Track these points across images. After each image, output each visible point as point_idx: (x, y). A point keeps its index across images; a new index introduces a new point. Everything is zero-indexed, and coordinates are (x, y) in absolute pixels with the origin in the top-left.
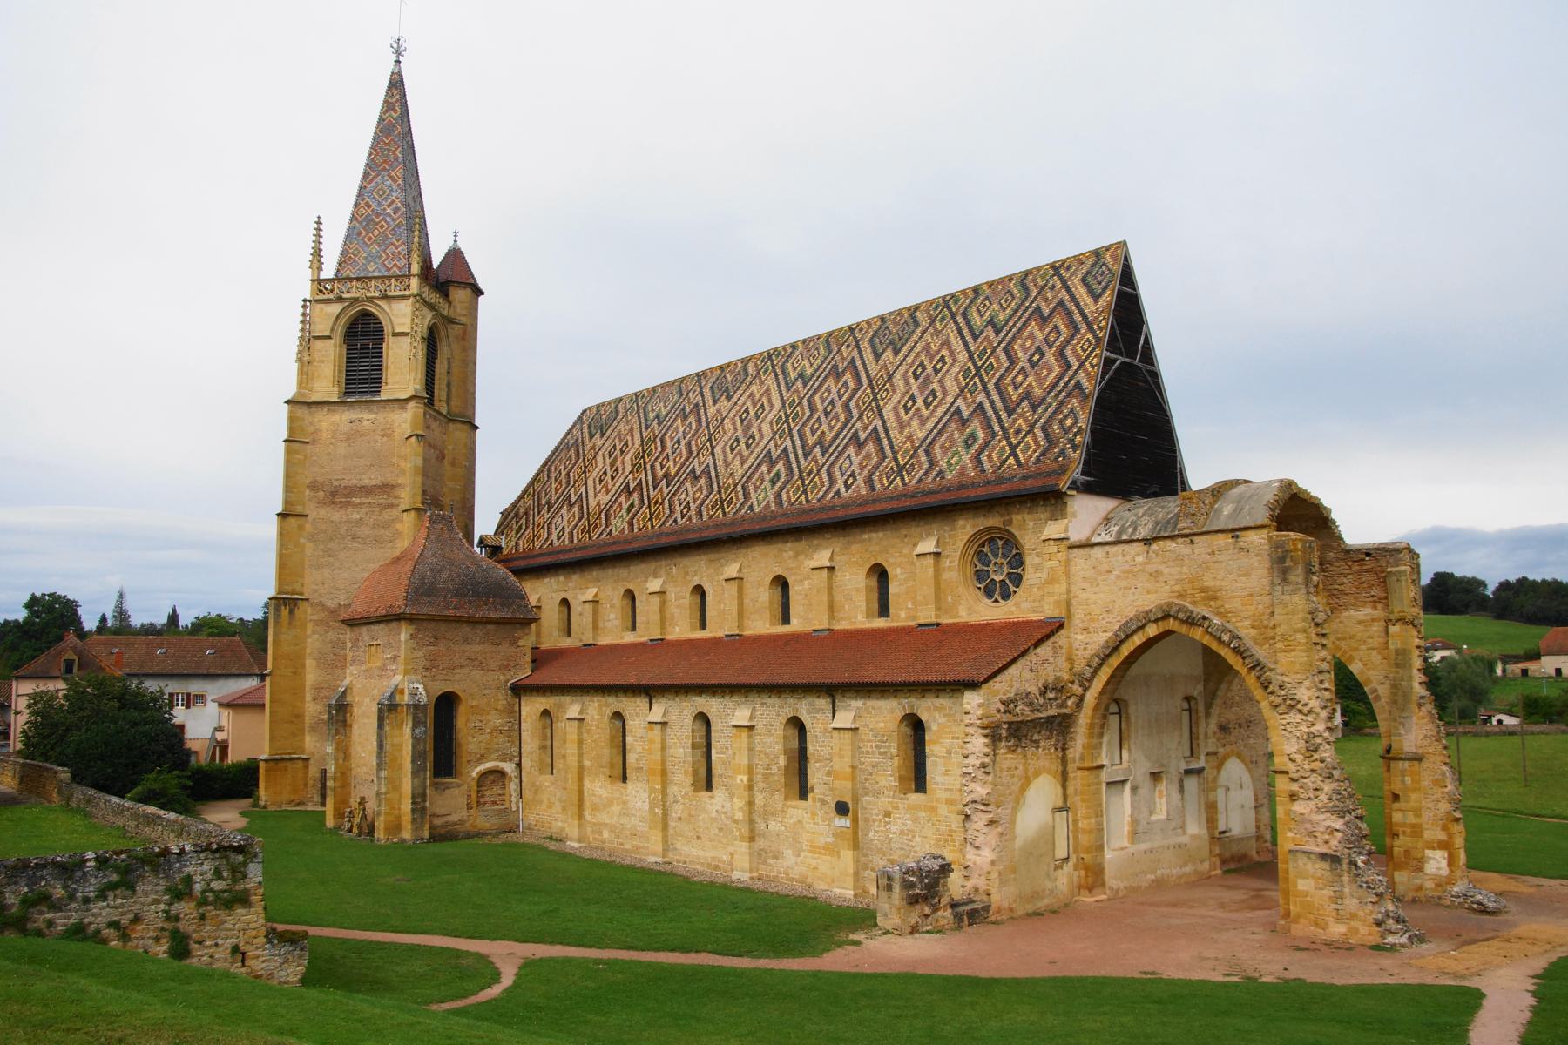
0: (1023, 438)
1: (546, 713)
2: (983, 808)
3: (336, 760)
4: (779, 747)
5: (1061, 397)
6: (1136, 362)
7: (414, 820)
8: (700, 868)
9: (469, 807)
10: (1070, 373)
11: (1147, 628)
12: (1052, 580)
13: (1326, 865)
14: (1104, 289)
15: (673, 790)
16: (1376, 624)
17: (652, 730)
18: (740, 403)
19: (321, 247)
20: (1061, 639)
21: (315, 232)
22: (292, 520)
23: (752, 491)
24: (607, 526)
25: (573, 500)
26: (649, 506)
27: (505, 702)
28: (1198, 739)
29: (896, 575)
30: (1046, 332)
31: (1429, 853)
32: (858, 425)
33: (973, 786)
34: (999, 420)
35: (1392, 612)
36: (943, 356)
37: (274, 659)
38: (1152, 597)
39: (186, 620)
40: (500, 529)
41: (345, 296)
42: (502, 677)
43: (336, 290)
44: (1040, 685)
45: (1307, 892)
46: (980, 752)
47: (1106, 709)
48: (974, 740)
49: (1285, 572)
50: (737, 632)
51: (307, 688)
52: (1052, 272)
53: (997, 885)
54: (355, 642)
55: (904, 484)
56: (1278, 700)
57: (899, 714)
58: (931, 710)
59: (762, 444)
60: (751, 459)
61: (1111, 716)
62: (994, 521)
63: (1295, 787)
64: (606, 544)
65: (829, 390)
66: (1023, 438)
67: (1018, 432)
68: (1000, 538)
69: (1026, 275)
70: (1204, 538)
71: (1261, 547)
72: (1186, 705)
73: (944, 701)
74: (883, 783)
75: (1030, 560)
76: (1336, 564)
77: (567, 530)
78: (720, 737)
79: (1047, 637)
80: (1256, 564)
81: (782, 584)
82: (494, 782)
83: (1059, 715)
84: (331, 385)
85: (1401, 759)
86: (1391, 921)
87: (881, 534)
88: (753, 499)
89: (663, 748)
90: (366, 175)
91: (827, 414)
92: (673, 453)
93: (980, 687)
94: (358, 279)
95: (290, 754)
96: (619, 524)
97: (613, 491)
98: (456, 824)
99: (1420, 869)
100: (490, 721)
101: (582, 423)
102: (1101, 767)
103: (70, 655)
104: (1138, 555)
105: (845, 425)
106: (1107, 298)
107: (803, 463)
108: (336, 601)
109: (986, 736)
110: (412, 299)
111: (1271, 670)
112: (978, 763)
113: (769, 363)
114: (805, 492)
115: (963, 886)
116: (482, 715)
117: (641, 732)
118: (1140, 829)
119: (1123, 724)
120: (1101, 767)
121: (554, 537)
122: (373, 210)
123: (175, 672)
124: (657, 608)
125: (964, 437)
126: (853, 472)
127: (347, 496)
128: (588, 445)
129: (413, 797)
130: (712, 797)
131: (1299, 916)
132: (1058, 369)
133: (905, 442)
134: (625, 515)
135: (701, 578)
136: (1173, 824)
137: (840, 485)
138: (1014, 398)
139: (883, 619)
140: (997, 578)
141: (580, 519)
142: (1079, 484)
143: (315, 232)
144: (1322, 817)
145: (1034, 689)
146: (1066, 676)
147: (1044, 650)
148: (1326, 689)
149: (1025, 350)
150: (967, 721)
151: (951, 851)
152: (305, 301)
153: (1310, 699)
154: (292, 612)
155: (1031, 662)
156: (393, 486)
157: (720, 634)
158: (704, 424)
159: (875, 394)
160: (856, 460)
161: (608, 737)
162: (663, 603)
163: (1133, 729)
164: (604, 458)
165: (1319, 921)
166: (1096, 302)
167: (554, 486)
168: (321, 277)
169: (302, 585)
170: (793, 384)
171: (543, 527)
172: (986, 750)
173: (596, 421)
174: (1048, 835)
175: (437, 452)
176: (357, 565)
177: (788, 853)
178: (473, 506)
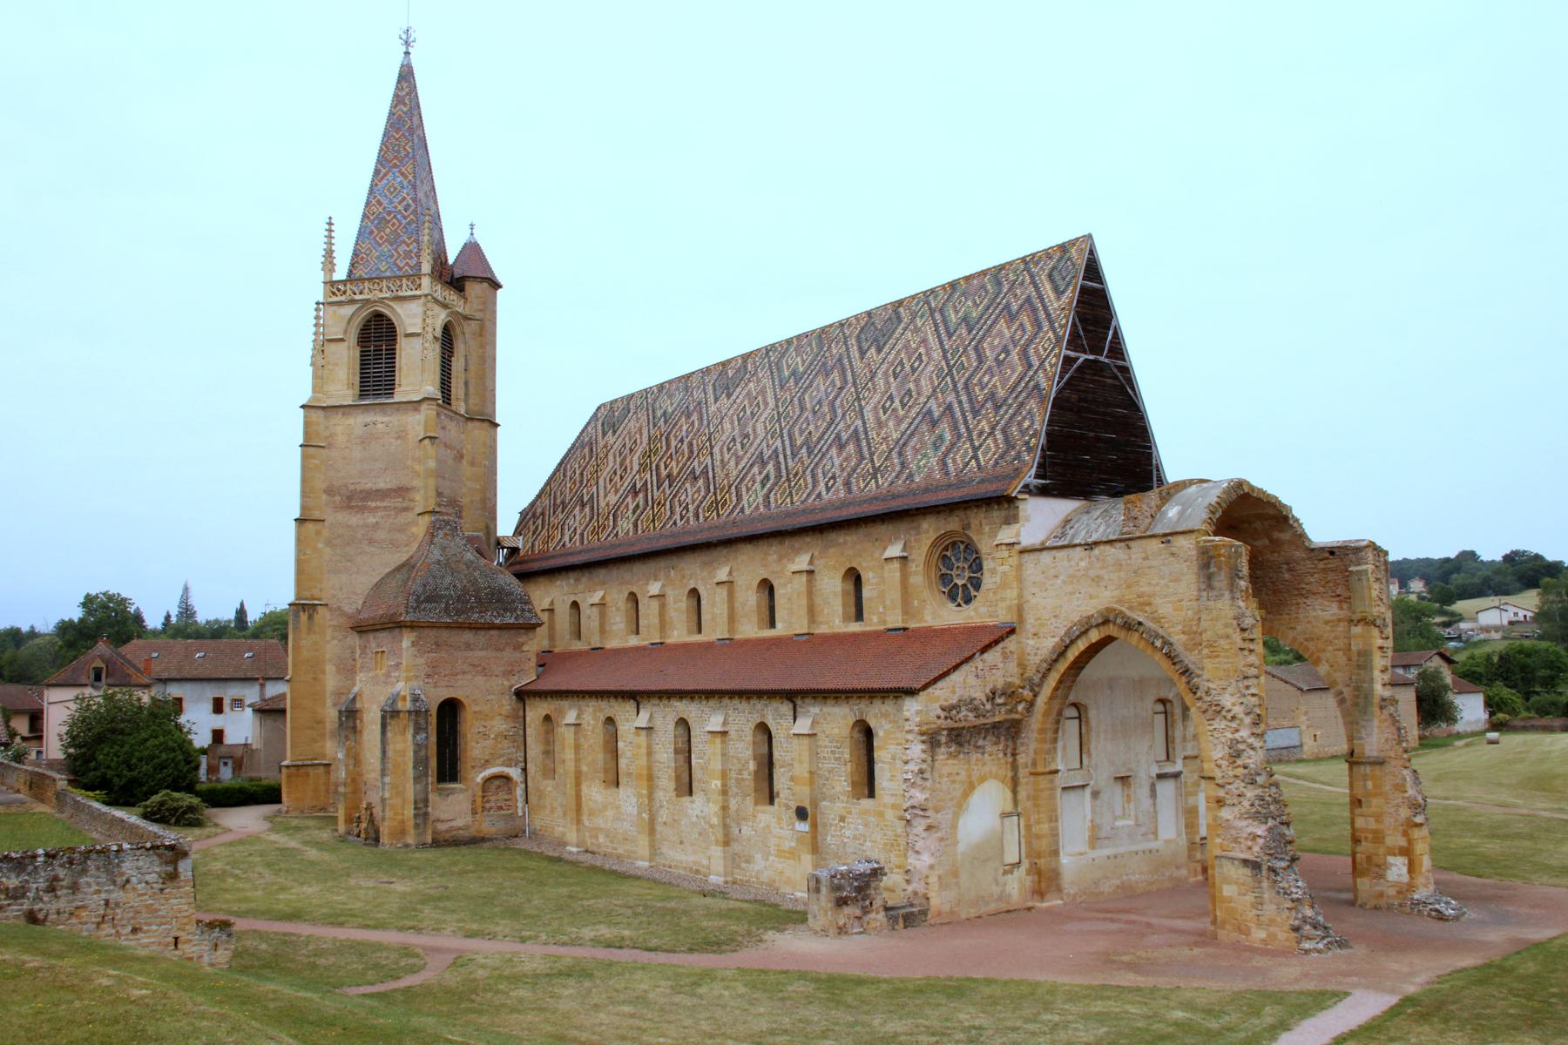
0: (985, 440)
1: (547, 718)
2: (921, 813)
3: (347, 766)
4: (749, 753)
5: (1020, 399)
6: (1102, 359)
7: (417, 826)
8: (682, 872)
9: (474, 812)
10: (1031, 373)
11: (1090, 633)
12: (1004, 585)
13: (1247, 871)
14: (1067, 286)
15: (659, 795)
16: (1341, 624)
17: (638, 735)
18: (738, 401)
19: (333, 248)
20: (1010, 644)
21: (326, 233)
22: (310, 526)
23: (744, 493)
24: (614, 528)
25: (585, 499)
26: (653, 508)
27: (509, 707)
28: (1173, 742)
29: (869, 579)
30: (1012, 330)
31: (1391, 859)
32: (842, 425)
33: (913, 792)
34: (966, 422)
35: (1354, 613)
36: (920, 354)
37: (294, 666)
38: (1094, 602)
39: (253, 616)
40: (518, 531)
41: (358, 297)
42: (506, 683)
43: (349, 292)
44: (988, 691)
45: (1231, 897)
46: (918, 758)
47: (1060, 713)
48: (913, 747)
49: (1209, 577)
50: (727, 636)
51: (328, 695)
52: (1022, 267)
53: (936, 889)
54: (364, 649)
55: (878, 487)
56: (1205, 706)
57: (851, 720)
58: (878, 715)
59: (755, 445)
60: (745, 460)
61: (1067, 721)
62: (952, 524)
63: (1221, 793)
64: (613, 546)
65: (818, 389)
66: (985, 440)
67: (981, 433)
68: (962, 542)
69: (1000, 270)
70: (1139, 542)
71: (1189, 553)
72: (1160, 708)
73: (888, 706)
74: (838, 789)
75: (986, 565)
76: (1302, 563)
77: (579, 531)
78: (699, 743)
79: (996, 642)
80: (1186, 570)
81: (767, 587)
82: (499, 787)
83: (1006, 720)
84: (345, 387)
85: (1363, 763)
86: (1308, 927)
87: (854, 538)
88: (745, 502)
89: (650, 754)
90: (377, 172)
91: (815, 413)
92: (676, 452)
93: (918, 694)
94: (370, 279)
95: (312, 759)
96: (625, 525)
97: (621, 492)
98: (460, 828)
99: (1382, 876)
100: (494, 726)
101: (597, 420)
102: (1057, 772)
103: (99, 664)
104: (1082, 559)
105: (830, 425)
106: (1071, 295)
107: (790, 464)
108: (354, 606)
109: (923, 742)
110: (423, 298)
111: (1198, 676)
112: (916, 769)
113: (766, 360)
114: (791, 494)
115: (904, 890)
116: (486, 720)
117: (631, 737)
118: (1103, 834)
119: (1083, 728)
120: (1057, 772)
121: (567, 538)
122: (384, 208)
123: (213, 676)
124: (656, 612)
125: (933, 438)
126: (834, 474)
127: (364, 499)
128: (601, 443)
129: (415, 802)
130: (693, 802)
131: (1224, 922)
132: (1020, 369)
133: (882, 444)
134: (759, 488)
135: (696, 582)
136: (1143, 830)
137: (821, 487)
138: (980, 399)
139: (858, 623)
140: (960, 582)
141: (590, 521)
142: (1031, 488)
143: (326, 233)
144: (1244, 823)
145: (979, 695)
146: (1017, 682)
147: (992, 656)
148: (1253, 695)
149: (993, 348)
150: (907, 728)
151: (897, 856)
152: (318, 303)
153: (1234, 705)
154: (310, 617)
155: (977, 668)
156: (408, 490)
157: (713, 637)
158: (705, 422)
159: (858, 394)
160: (837, 462)
161: (602, 742)
162: (663, 607)
163: (1093, 734)
164: (615, 457)
165: (1243, 927)
166: (1058, 299)
167: (568, 485)
168: (335, 279)
169: (321, 590)
170: (787, 382)
171: (557, 528)
172: (924, 756)
173: (609, 417)
174: (996, 844)
175: (455, 452)
176: (374, 570)
177: (758, 857)
178: (495, 505)
